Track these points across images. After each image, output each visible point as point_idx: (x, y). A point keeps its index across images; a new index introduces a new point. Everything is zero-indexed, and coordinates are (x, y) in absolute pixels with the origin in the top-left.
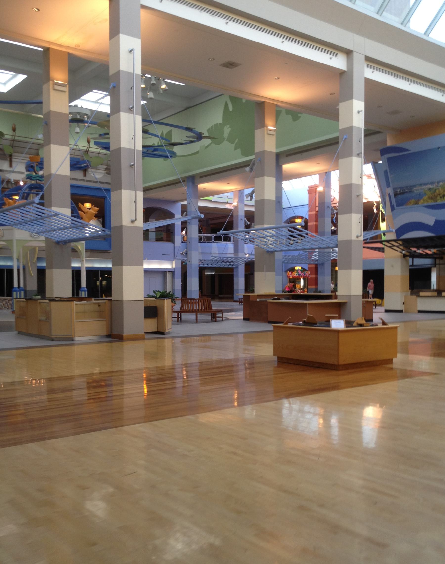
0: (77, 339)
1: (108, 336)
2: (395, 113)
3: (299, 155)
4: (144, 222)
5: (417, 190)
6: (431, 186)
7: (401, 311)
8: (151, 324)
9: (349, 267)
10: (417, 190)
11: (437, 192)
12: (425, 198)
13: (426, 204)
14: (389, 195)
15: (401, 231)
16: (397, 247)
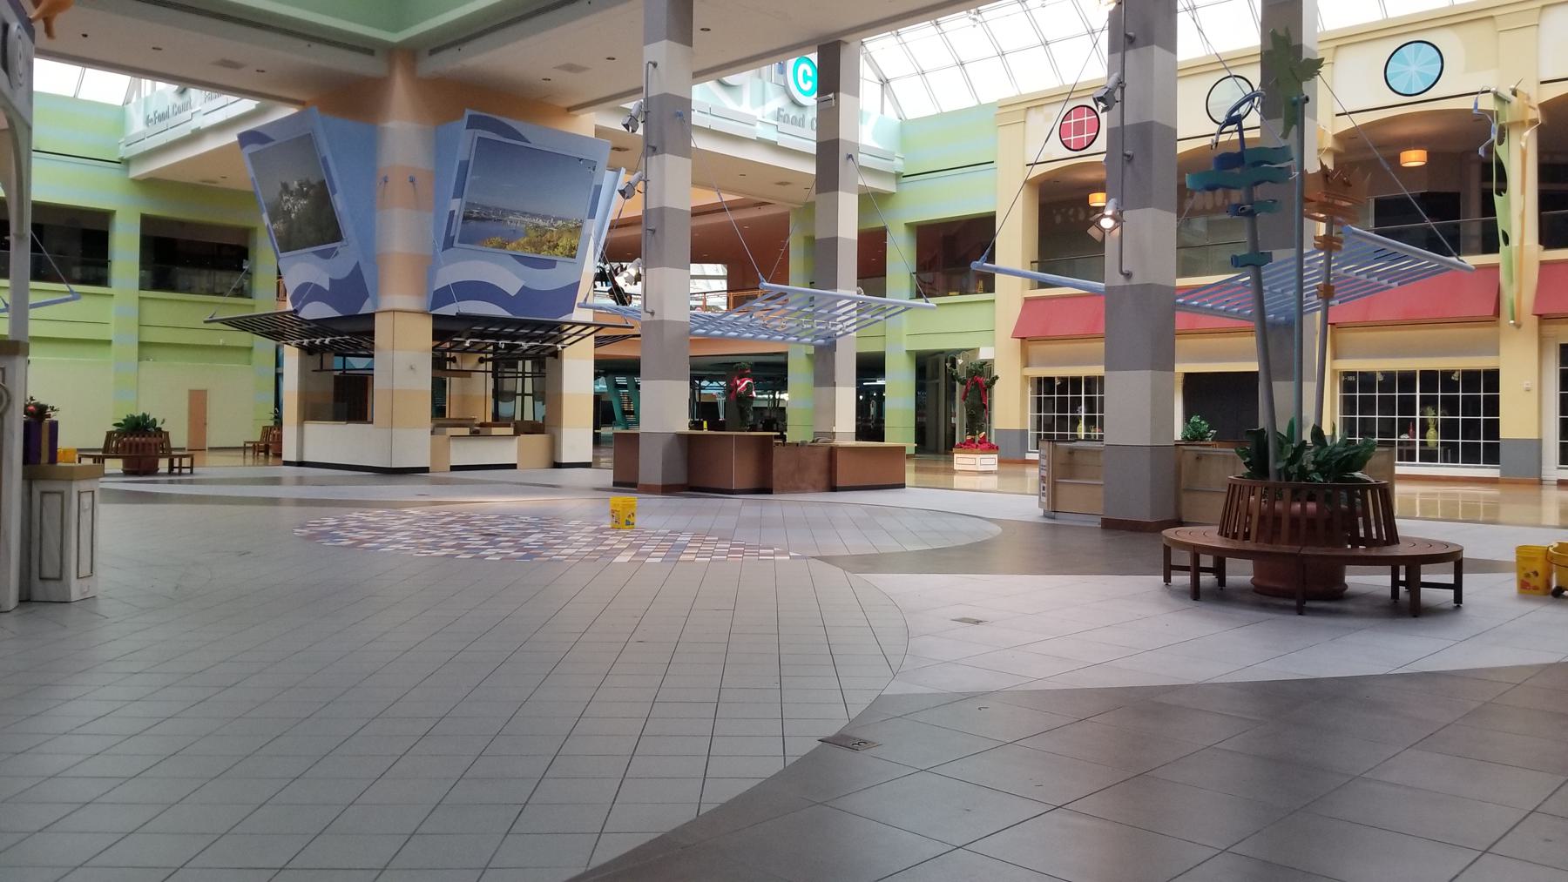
4: (143, 286)
5: (514, 221)
6: (541, 222)
10: (514, 221)
12: (523, 241)
13: (520, 253)
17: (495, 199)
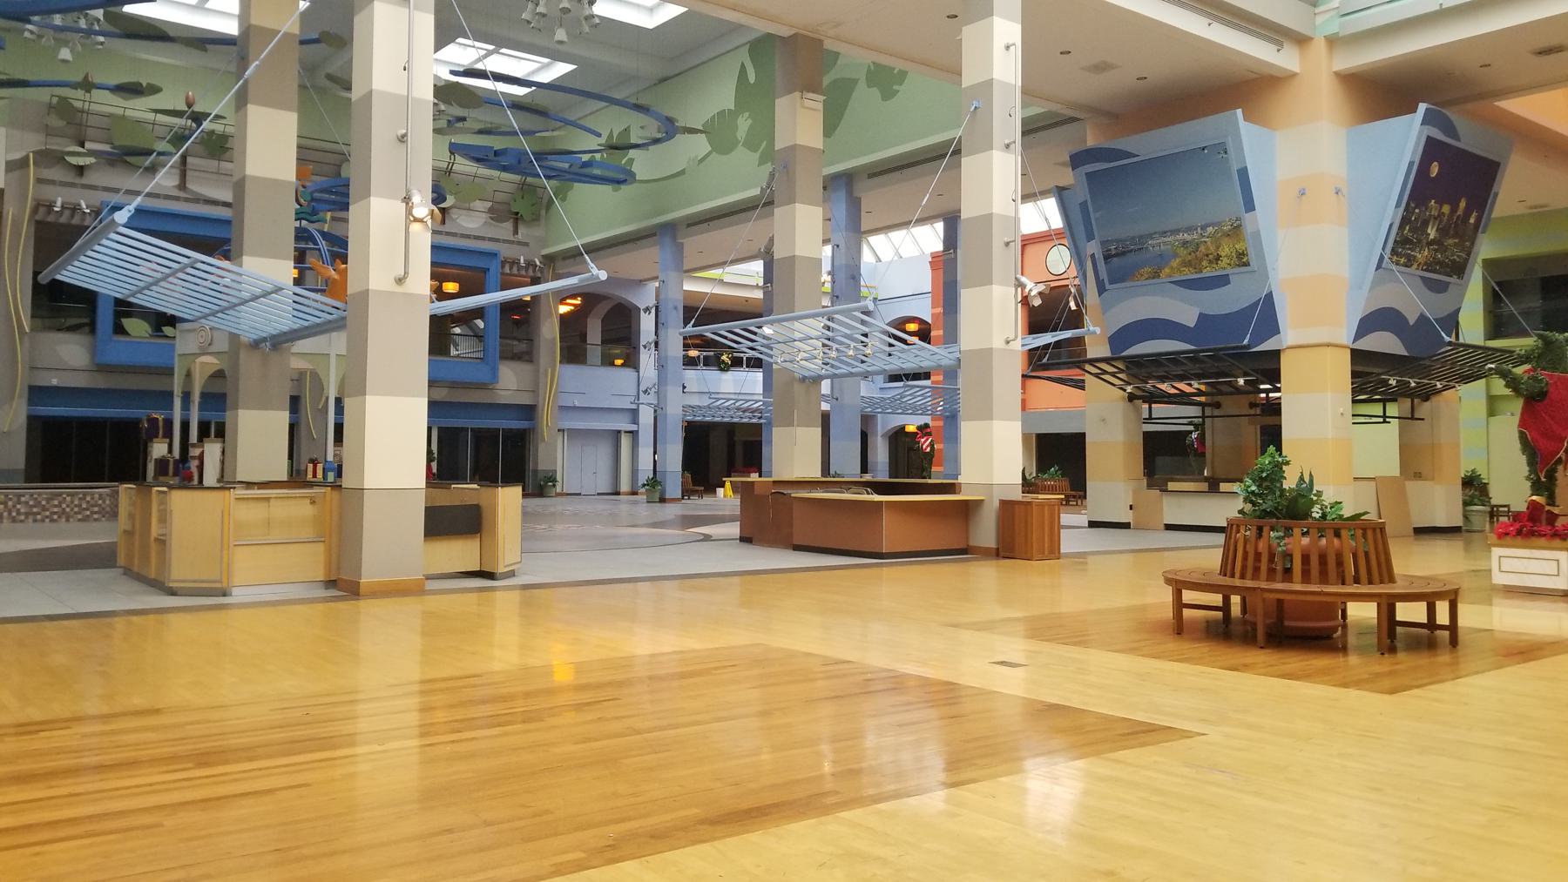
0: (239, 595)
1: (331, 583)
2: (1100, 68)
3: (897, 175)
5: (1158, 245)
7: (1126, 526)
8: (460, 553)
9: (986, 414)
10: (1158, 245)
11: (1202, 248)
12: (1175, 263)
14: (1093, 256)
15: (1120, 339)
16: (1113, 374)
17: (1126, 230)
